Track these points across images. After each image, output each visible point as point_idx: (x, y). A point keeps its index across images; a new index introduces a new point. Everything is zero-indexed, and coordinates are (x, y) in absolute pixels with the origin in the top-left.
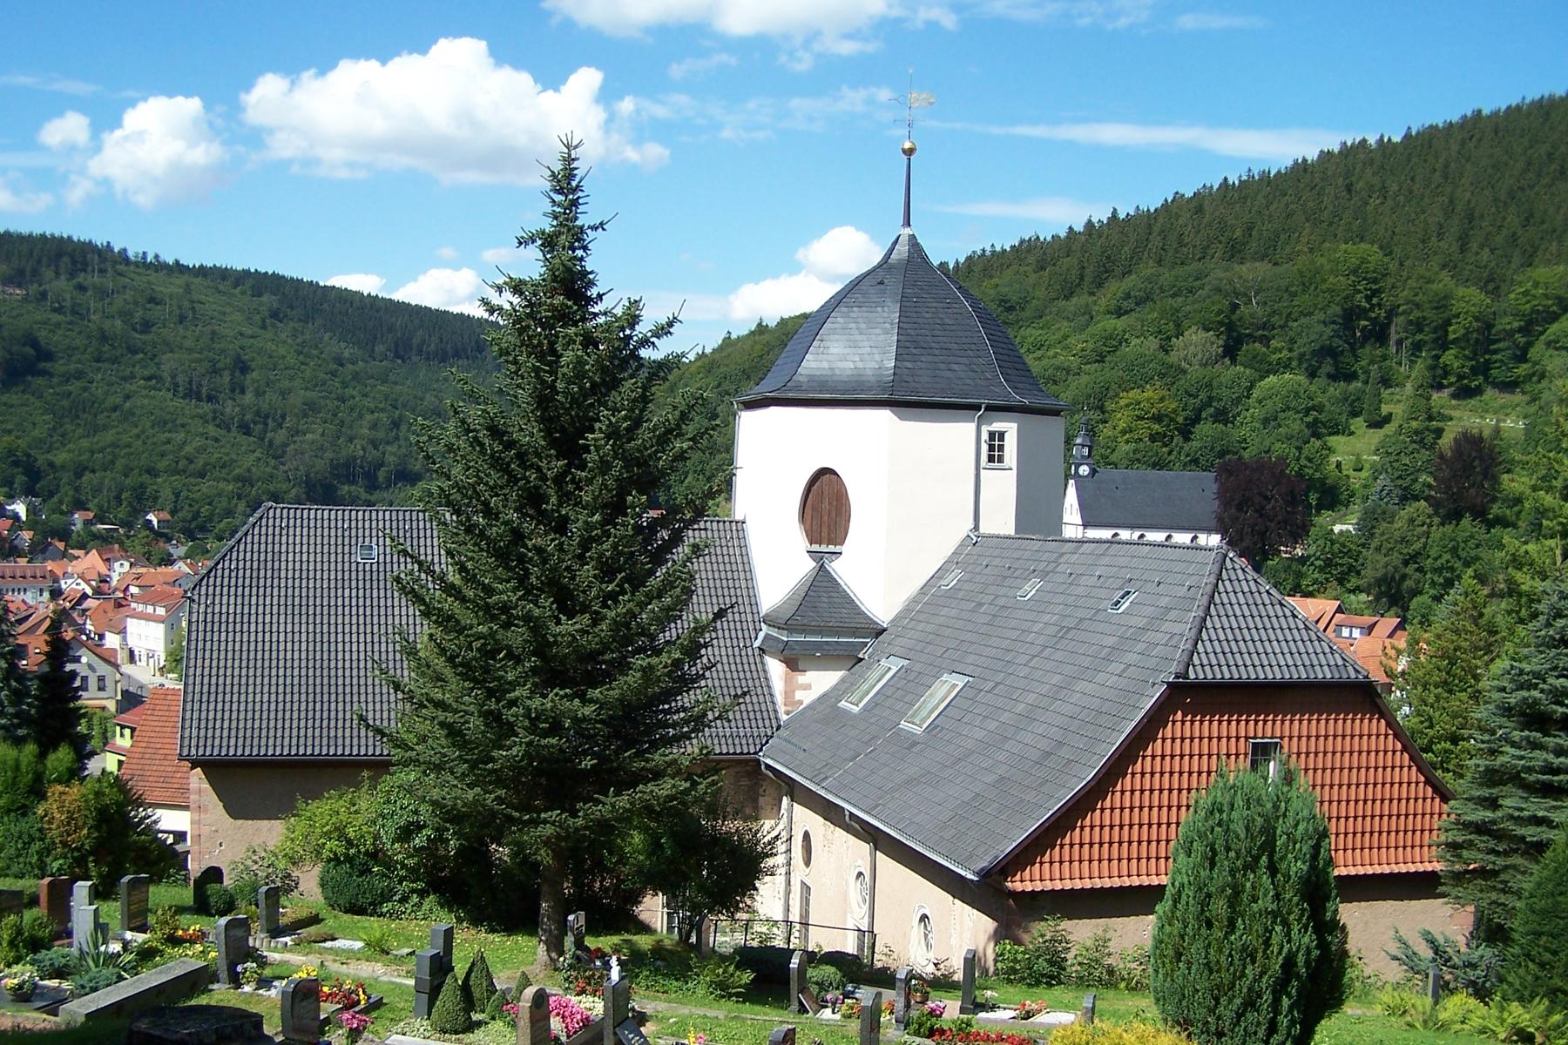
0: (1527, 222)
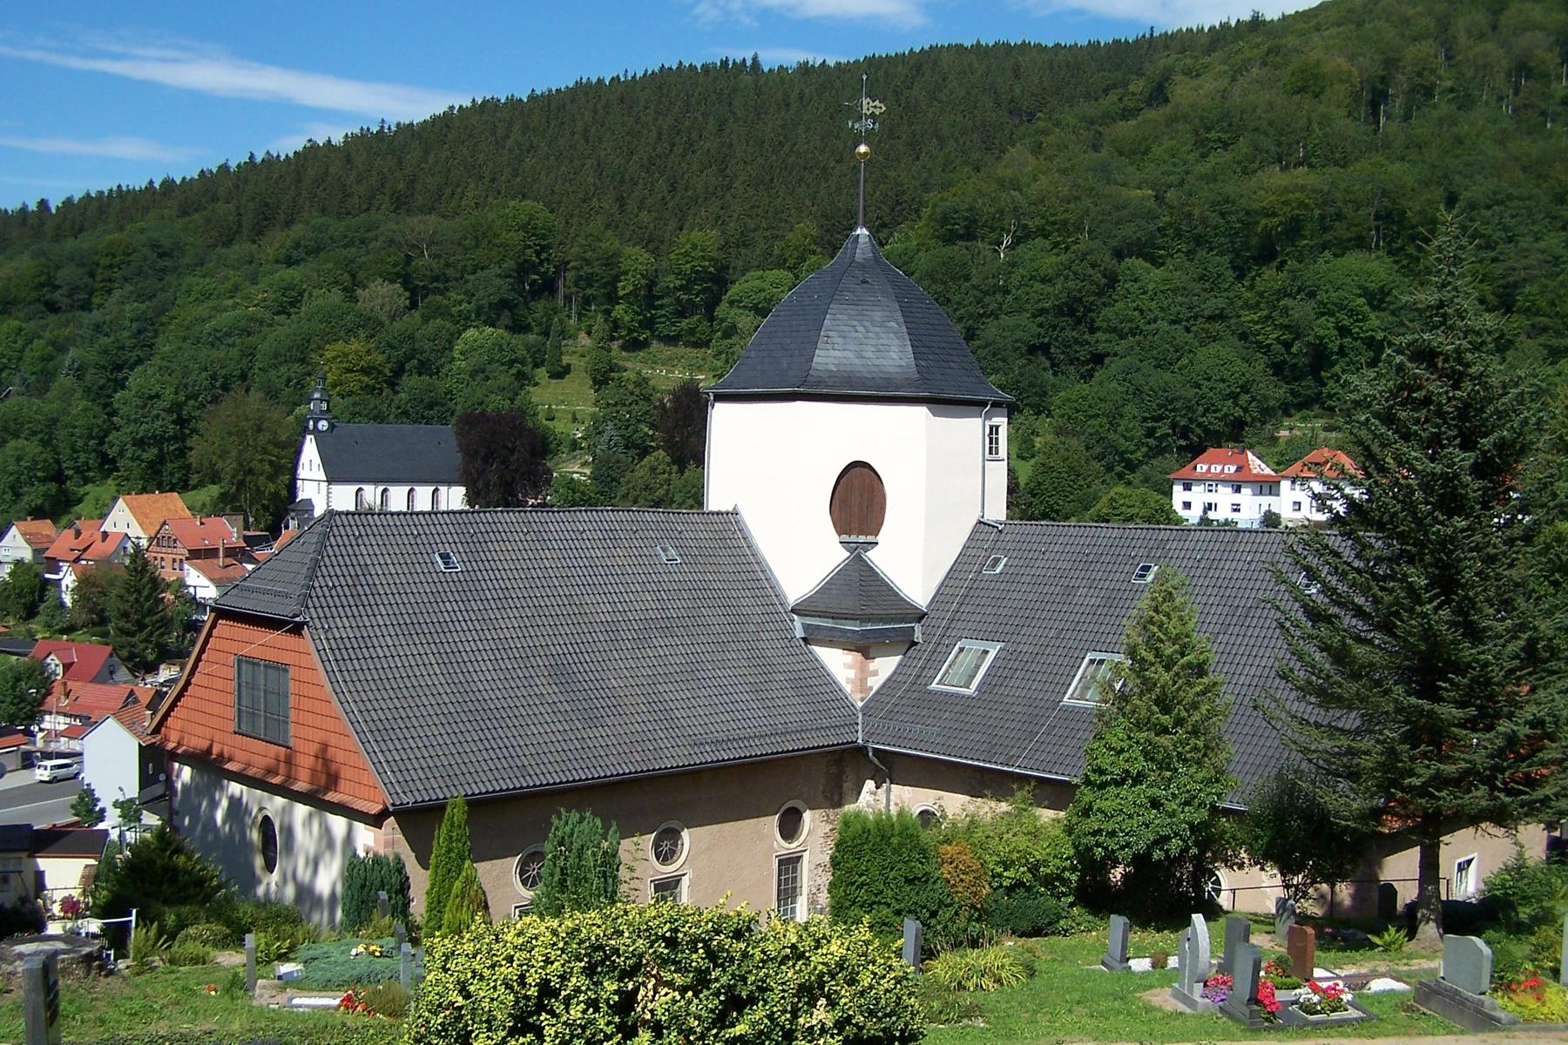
0: (673, 189)
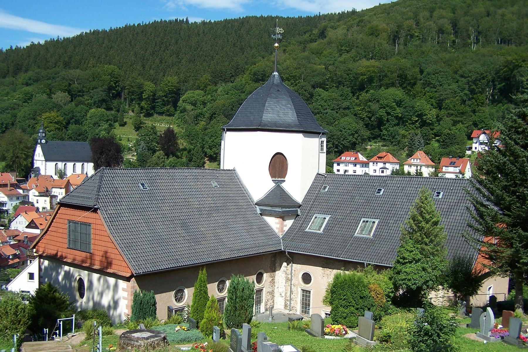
0: (161, 62)
